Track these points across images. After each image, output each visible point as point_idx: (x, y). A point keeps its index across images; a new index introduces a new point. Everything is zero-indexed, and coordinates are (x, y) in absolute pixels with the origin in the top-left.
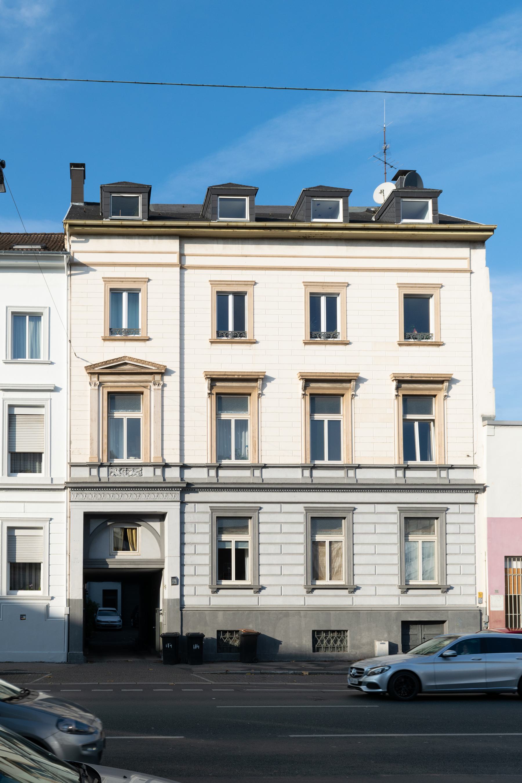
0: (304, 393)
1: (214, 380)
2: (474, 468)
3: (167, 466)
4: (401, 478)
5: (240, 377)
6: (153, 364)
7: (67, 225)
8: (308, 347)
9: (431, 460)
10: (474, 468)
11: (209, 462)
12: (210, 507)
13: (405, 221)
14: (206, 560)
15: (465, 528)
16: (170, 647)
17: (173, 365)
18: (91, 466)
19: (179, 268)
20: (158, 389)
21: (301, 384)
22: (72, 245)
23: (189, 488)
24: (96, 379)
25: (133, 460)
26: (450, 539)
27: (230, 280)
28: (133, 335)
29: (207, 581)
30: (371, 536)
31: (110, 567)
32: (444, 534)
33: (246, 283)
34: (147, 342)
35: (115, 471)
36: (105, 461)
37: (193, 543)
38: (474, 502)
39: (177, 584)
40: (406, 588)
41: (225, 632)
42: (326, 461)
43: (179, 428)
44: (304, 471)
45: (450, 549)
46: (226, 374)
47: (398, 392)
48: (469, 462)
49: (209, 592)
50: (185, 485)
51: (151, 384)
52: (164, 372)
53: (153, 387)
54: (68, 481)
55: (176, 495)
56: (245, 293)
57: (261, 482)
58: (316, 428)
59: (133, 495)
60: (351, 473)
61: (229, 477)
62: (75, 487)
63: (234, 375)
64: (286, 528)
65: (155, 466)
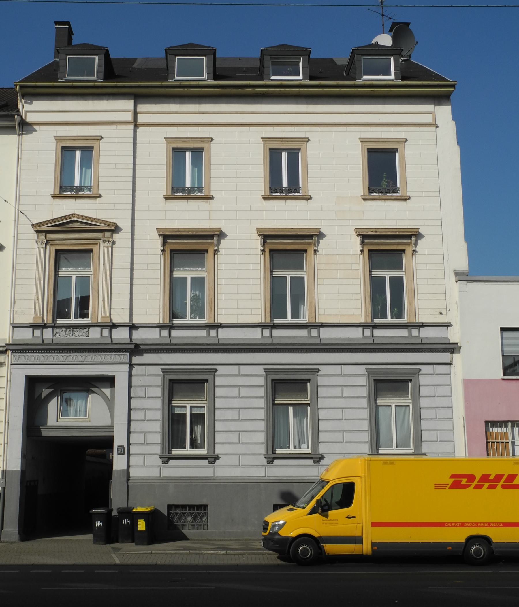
0: (262, 248)
1: (166, 236)
2: (448, 325)
3: (113, 326)
4: (369, 337)
5: (195, 233)
6: (102, 221)
7: (18, 87)
8: (267, 202)
9: (304, 318)
10: (448, 325)
11: (161, 322)
12: (162, 369)
13: (365, 77)
14: (157, 427)
15: (441, 391)
16: (128, 523)
17: (123, 220)
18: (34, 326)
19: (133, 126)
20: (108, 247)
21: (258, 240)
22: (25, 105)
23: (136, 349)
24: (43, 237)
25: (198, 321)
26: (424, 402)
27: (187, 136)
28: (293, 194)
29: (157, 450)
30: (337, 400)
31: (43, 434)
32: (418, 397)
33: (202, 139)
34: (98, 199)
35: (62, 332)
36: (50, 321)
37: (143, 409)
38: (449, 362)
39: (124, 454)
40: (272, 458)
41: (177, 507)
42: (389, 320)
43: (131, 288)
44: (264, 330)
45: (424, 413)
46: (180, 230)
47: (362, 247)
48: (442, 320)
49: (160, 462)
50: (133, 347)
51: (101, 241)
52: (115, 229)
53: (102, 245)
54: (10, 342)
55: (125, 357)
56: (299, 149)
57: (217, 342)
58: (376, 286)
59: (79, 357)
60: (213, 333)
61: (183, 337)
62: (18, 349)
63: (188, 232)
64: (244, 392)
65: (103, 326)
